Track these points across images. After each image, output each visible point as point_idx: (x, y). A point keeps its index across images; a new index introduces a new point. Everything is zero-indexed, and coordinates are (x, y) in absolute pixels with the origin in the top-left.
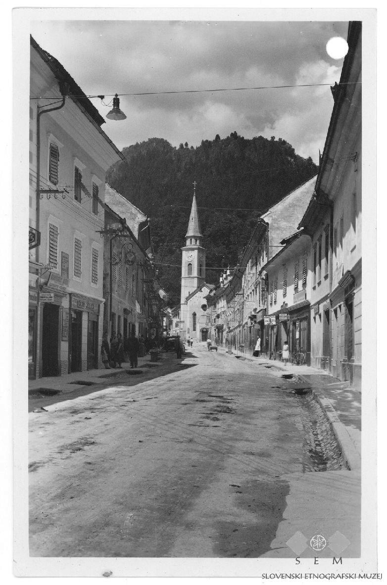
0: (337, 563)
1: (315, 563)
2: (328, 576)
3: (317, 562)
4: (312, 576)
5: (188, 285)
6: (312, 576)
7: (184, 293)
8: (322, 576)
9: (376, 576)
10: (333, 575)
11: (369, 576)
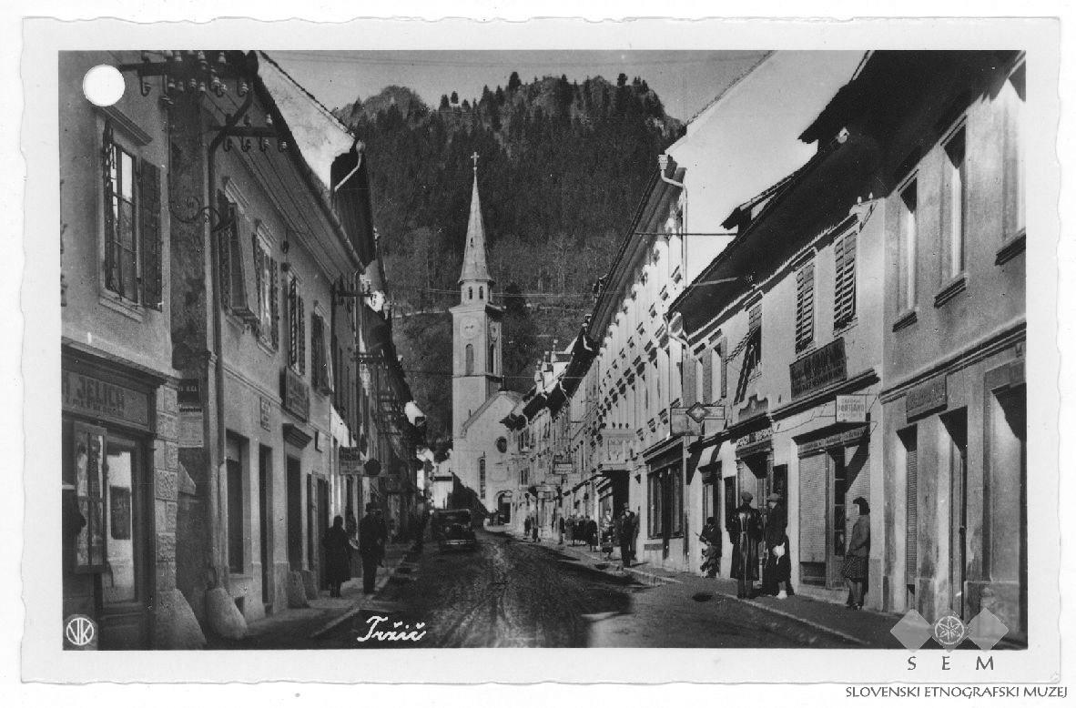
0: (984, 667)
1: (944, 668)
2: (968, 692)
3: (946, 666)
4: (938, 691)
5: (466, 392)
6: (938, 691)
7: (459, 416)
8: (956, 692)
9: (1059, 692)
10: (977, 690)
11: (1042, 692)
